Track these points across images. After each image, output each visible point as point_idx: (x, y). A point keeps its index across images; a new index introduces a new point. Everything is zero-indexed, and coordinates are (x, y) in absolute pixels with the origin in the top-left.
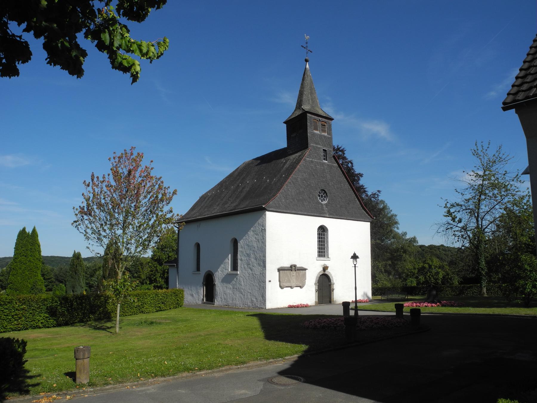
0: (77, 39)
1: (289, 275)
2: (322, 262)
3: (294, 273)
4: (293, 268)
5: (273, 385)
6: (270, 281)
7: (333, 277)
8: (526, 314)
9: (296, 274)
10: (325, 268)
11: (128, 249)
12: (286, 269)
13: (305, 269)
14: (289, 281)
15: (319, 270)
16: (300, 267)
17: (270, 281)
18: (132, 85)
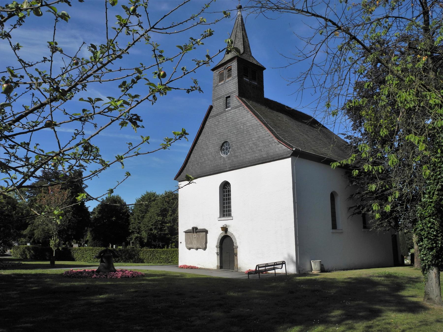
1: (191, 237)
2: (223, 223)
3: (195, 235)
6: (181, 243)
7: (237, 239)
9: (197, 236)
10: (225, 229)
18: (177, 46)
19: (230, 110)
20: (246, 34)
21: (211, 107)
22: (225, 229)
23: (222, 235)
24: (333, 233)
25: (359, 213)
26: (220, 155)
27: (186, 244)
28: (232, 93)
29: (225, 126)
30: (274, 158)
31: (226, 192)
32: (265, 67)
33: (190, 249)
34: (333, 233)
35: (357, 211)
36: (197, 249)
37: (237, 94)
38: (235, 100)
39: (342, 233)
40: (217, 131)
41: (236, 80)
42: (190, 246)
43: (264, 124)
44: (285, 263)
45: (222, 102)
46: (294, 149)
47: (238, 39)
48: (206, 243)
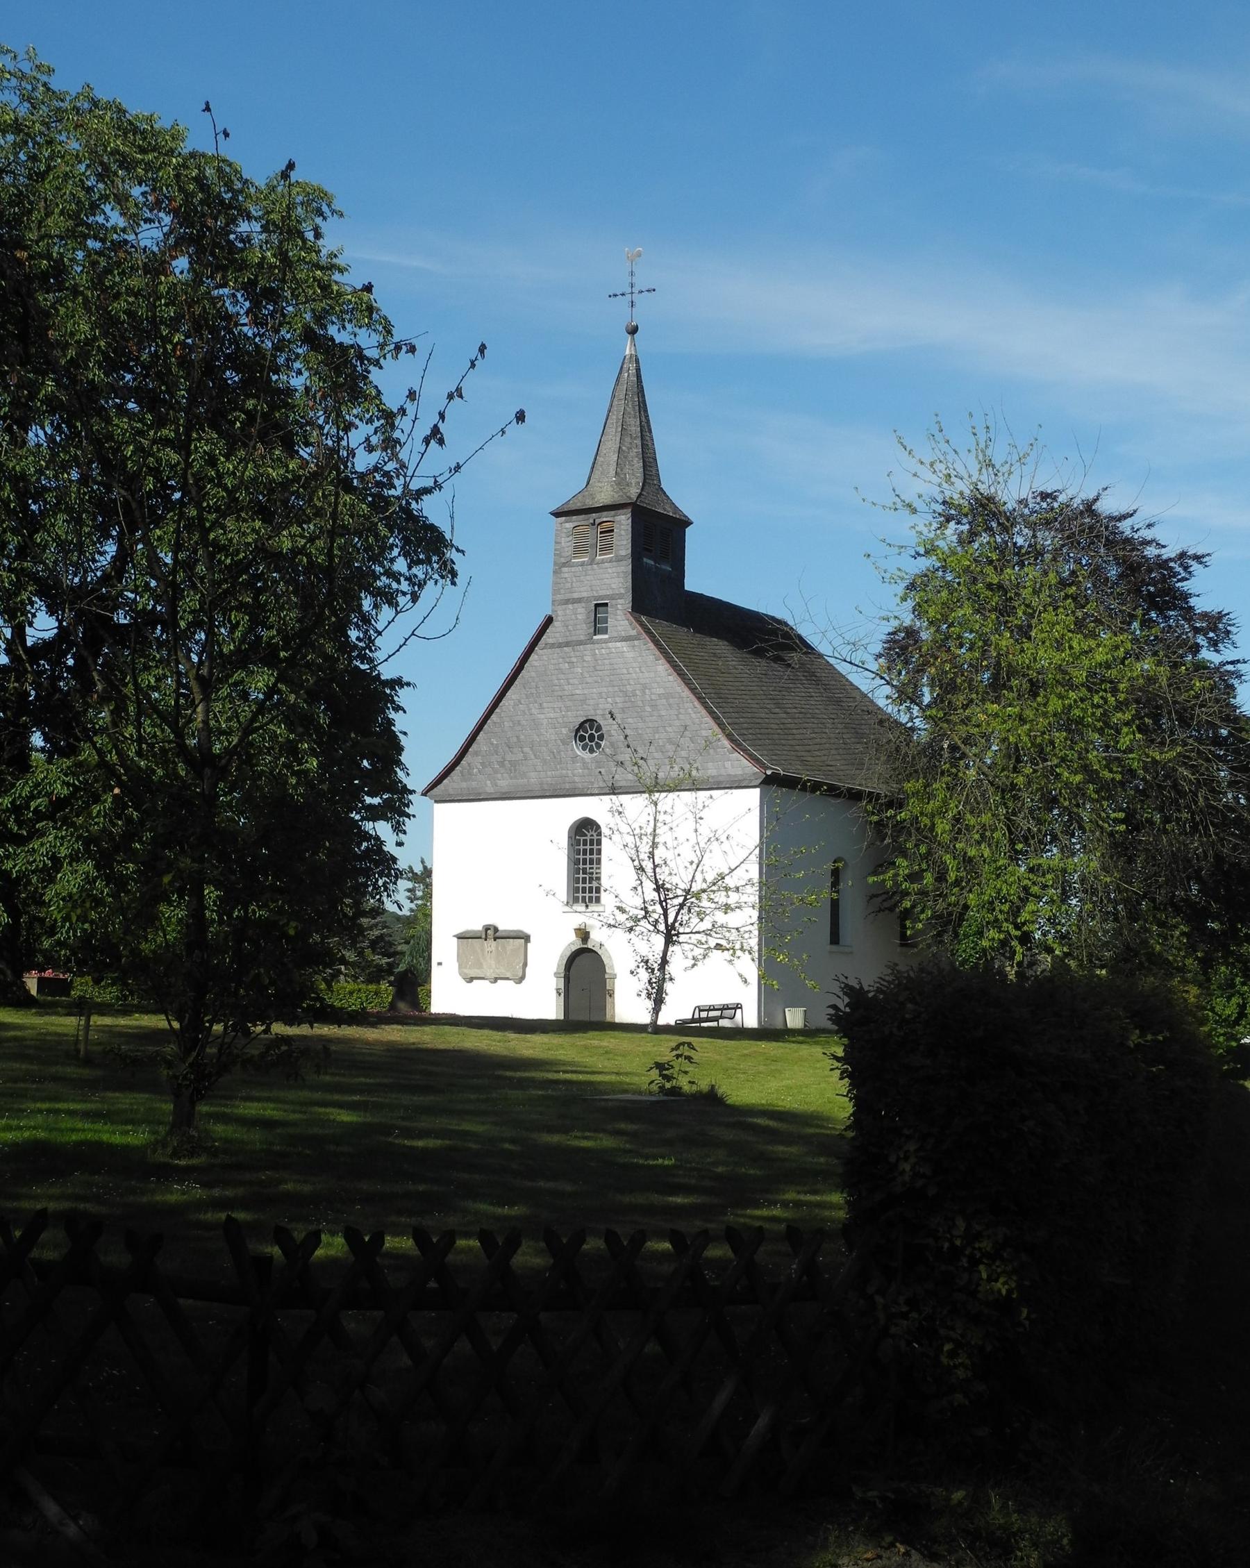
0: (1193, 601)
3: (491, 945)
4: (491, 933)
5: (693, 1181)
6: (440, 964)
8: (15, 1081)
9: (497, 948)
10: (583, 934)
11: (917, 846)
12: (512, 934)
13: (527, 938)
14: (480, 966)
15: (567, 941)
16: (505, 931)
17: (440, 964)
19: (605, 641)
20: (649, 426)
21: (549, 621)
22: (583, 934)
23: (574, 948)
24: (831, 952)
25: (891, 909)
26: (573, 750)
27: (460, 967)
28: (612, 597)
29: (589, 680)
30: (719, 783)
31: (585, 844)
32: (691, 518)
33: (470, 980)
34: (831, 952)
35: (886, 905)
36: (495, 980)
37: (625, 603)
38: (621, 619)
39: (851, 953)
40: (566, 687)
41: (626, 567)
42: (473, 973)
43: (699, 698)
44: (741, 1008)
45: (582, 614)
46: (769, 772)
47: (628, 439)
48: (525, 965)
